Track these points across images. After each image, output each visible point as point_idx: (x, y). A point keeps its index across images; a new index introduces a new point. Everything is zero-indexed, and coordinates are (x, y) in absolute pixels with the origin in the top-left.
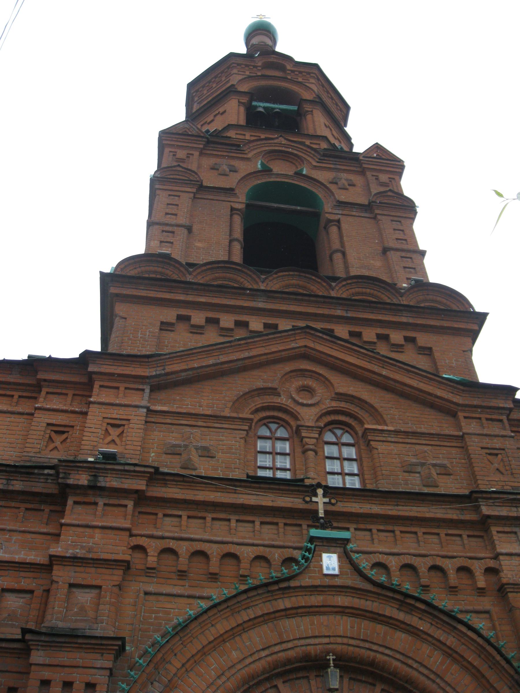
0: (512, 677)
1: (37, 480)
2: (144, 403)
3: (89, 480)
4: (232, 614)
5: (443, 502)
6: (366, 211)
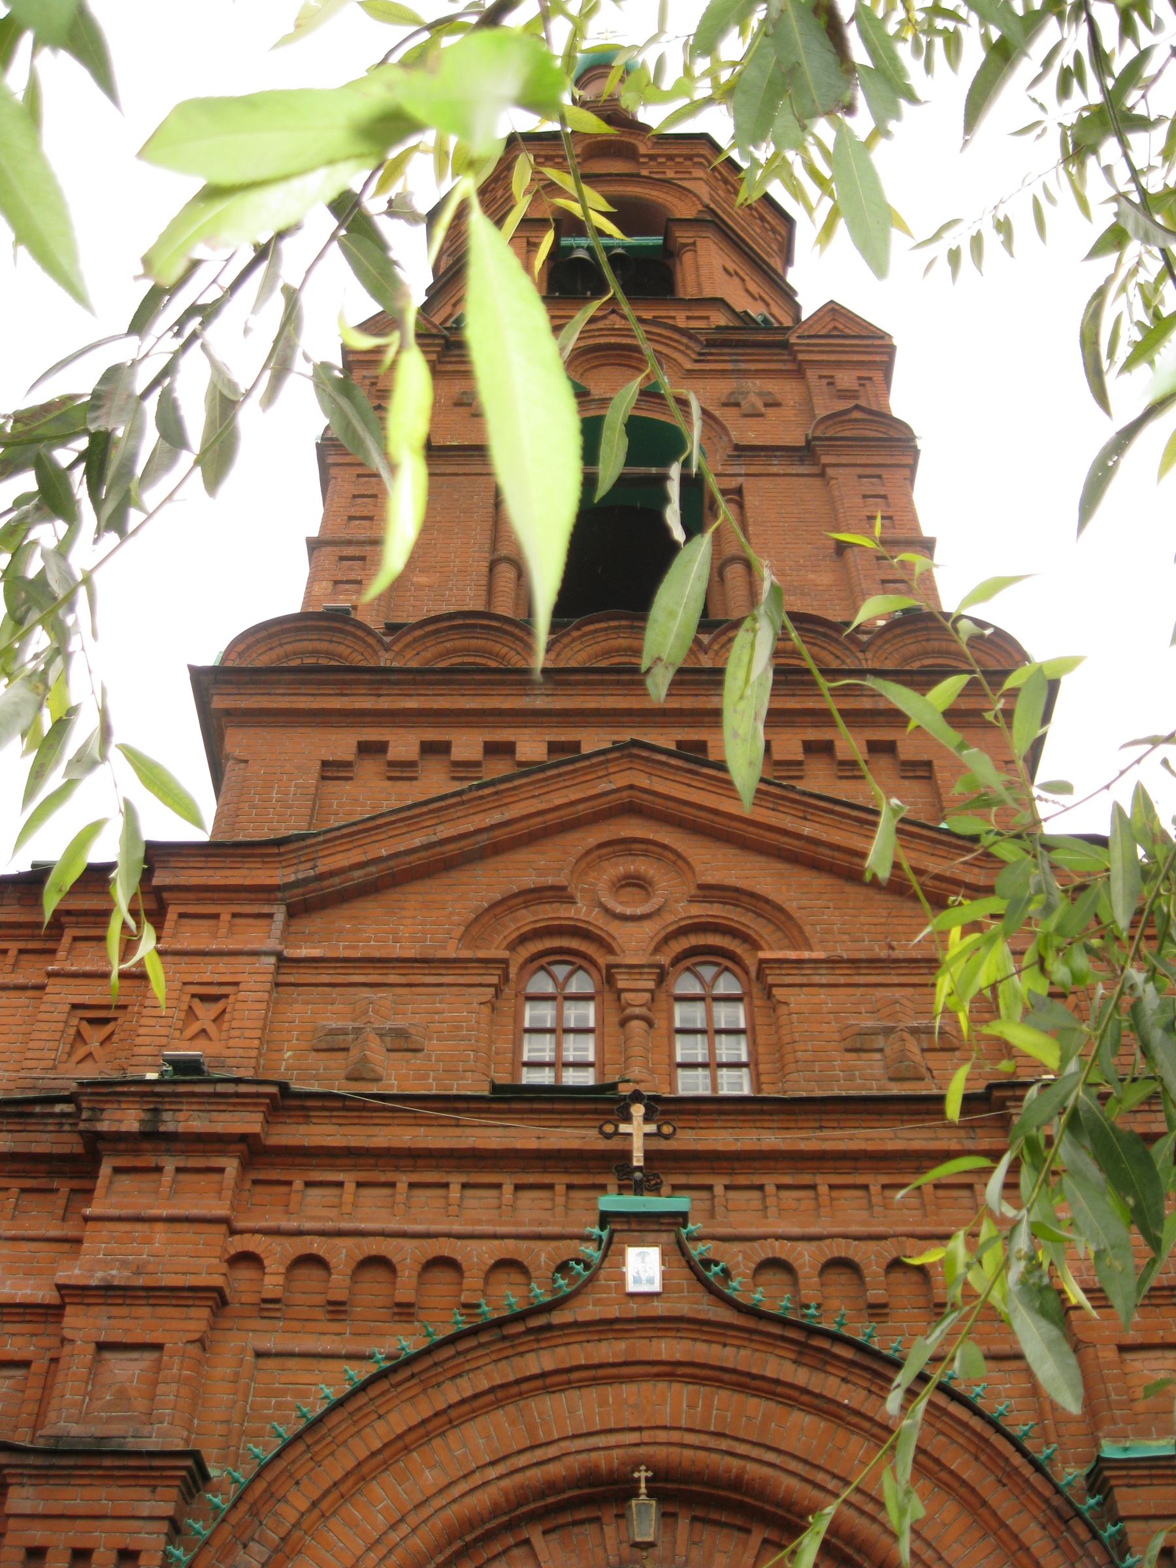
0: (1047, 1501)
1: (41, 1128)
2: (272, 944)
3: (141, 1121)
4: (425, 1390)
5: (927, 1113)
6: (802, 461)
